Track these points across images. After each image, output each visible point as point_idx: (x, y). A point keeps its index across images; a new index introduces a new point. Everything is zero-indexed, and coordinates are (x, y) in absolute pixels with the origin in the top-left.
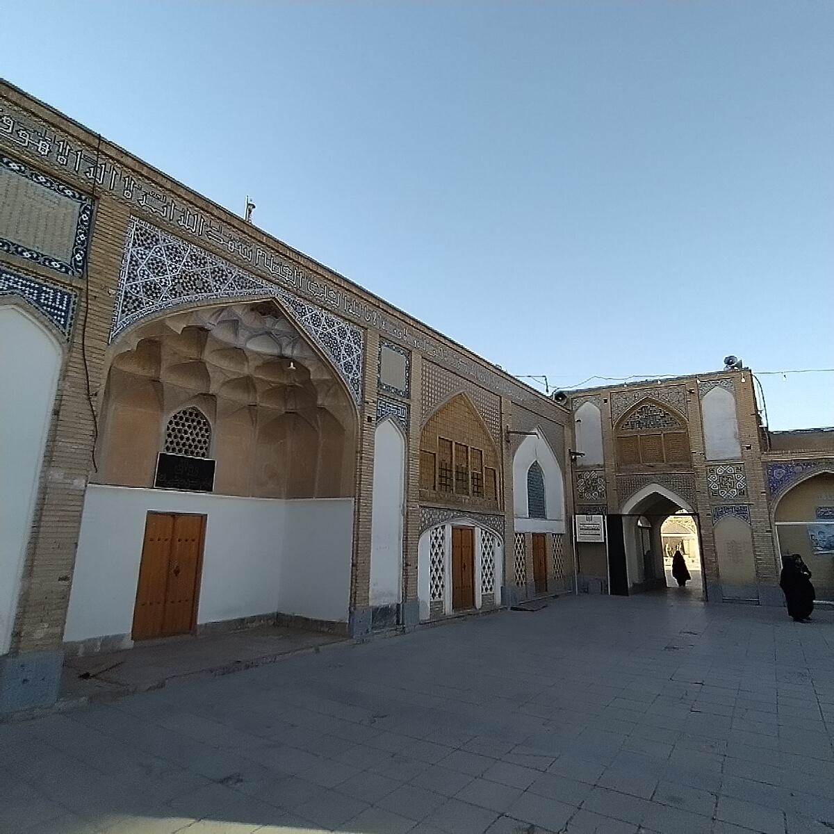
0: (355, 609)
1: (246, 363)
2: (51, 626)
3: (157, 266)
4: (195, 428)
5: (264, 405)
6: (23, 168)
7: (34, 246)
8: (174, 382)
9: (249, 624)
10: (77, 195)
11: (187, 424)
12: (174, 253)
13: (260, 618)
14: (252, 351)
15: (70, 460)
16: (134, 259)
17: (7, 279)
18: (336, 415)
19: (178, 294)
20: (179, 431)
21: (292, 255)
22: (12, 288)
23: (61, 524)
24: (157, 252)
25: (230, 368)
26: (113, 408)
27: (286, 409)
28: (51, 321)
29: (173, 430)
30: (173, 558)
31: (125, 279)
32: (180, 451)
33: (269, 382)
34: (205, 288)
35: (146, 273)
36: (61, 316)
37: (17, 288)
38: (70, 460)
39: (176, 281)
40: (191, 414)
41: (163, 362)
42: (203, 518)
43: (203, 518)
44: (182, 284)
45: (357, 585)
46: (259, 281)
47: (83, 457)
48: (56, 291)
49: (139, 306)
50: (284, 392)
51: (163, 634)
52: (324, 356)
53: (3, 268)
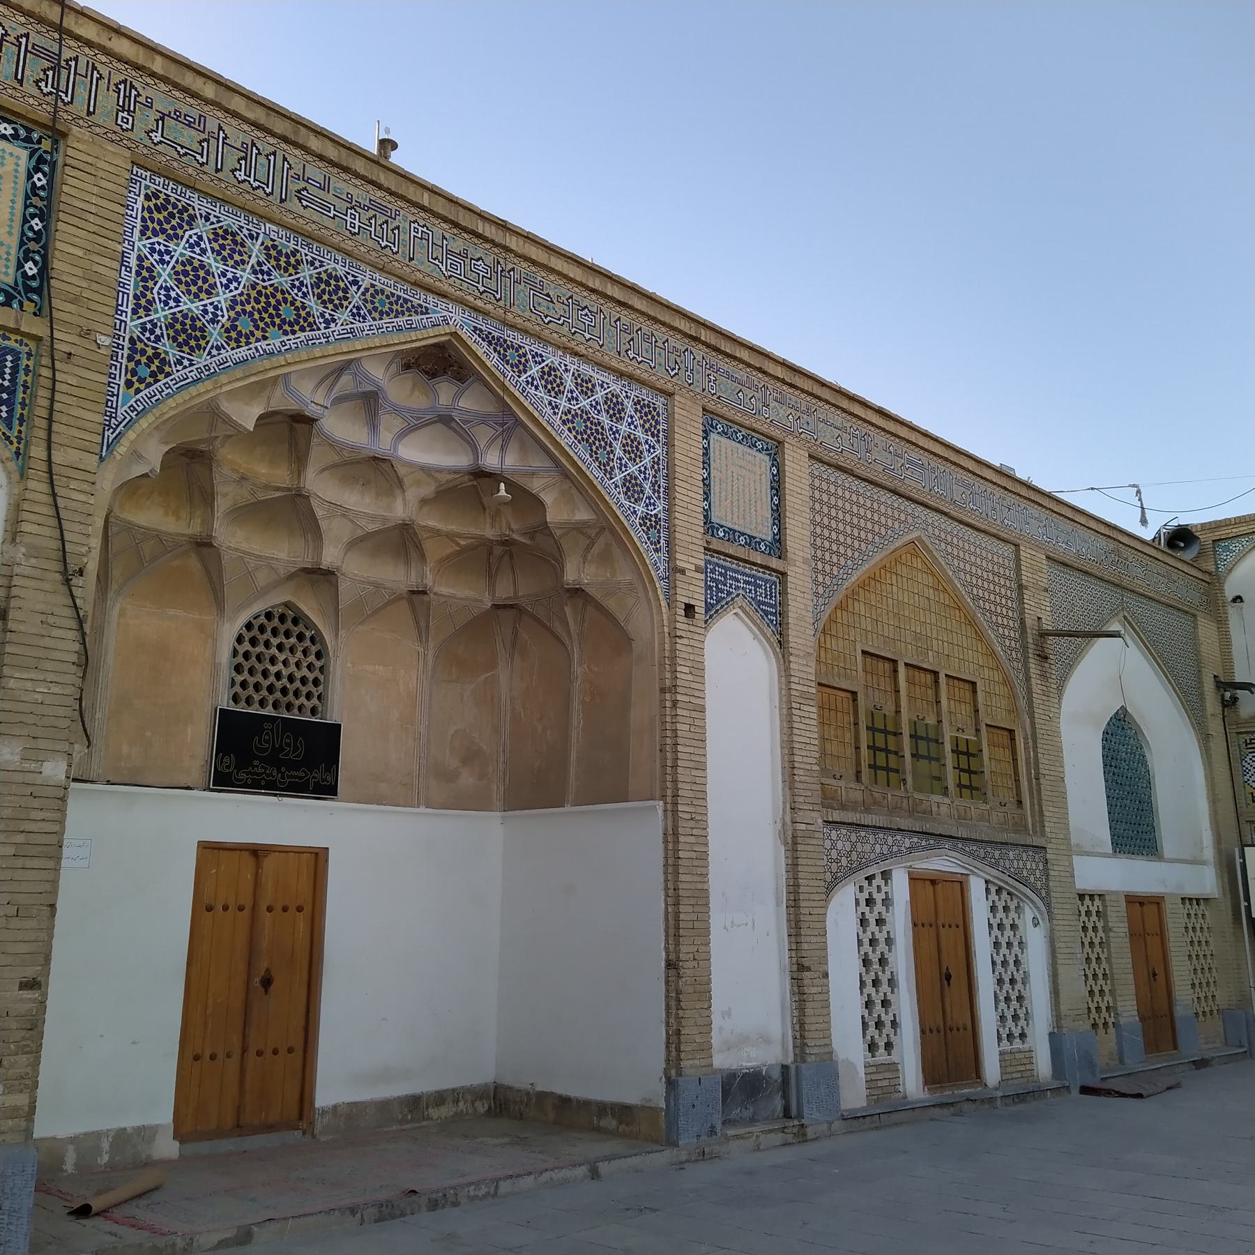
1: (398, 492)
5: (444, 590)
8: (244, 546)
10: (22, 132)
12: (229, 244)
14: (410, 464)
15: (30, 719)
18: (610, 604)
21: (490, 231)
23: (19, 862)
26: (116, 612)
29: (247, 655)
31: (129, 311)
32: (249, 701)
34: (303, 321)
40: (282, 618)
42: (318, 857)
43: (318, 857)
44: (251, 314)
46: (419, 298)
49: (161, 370)
50: (489, 558)
51: (240, 1129)
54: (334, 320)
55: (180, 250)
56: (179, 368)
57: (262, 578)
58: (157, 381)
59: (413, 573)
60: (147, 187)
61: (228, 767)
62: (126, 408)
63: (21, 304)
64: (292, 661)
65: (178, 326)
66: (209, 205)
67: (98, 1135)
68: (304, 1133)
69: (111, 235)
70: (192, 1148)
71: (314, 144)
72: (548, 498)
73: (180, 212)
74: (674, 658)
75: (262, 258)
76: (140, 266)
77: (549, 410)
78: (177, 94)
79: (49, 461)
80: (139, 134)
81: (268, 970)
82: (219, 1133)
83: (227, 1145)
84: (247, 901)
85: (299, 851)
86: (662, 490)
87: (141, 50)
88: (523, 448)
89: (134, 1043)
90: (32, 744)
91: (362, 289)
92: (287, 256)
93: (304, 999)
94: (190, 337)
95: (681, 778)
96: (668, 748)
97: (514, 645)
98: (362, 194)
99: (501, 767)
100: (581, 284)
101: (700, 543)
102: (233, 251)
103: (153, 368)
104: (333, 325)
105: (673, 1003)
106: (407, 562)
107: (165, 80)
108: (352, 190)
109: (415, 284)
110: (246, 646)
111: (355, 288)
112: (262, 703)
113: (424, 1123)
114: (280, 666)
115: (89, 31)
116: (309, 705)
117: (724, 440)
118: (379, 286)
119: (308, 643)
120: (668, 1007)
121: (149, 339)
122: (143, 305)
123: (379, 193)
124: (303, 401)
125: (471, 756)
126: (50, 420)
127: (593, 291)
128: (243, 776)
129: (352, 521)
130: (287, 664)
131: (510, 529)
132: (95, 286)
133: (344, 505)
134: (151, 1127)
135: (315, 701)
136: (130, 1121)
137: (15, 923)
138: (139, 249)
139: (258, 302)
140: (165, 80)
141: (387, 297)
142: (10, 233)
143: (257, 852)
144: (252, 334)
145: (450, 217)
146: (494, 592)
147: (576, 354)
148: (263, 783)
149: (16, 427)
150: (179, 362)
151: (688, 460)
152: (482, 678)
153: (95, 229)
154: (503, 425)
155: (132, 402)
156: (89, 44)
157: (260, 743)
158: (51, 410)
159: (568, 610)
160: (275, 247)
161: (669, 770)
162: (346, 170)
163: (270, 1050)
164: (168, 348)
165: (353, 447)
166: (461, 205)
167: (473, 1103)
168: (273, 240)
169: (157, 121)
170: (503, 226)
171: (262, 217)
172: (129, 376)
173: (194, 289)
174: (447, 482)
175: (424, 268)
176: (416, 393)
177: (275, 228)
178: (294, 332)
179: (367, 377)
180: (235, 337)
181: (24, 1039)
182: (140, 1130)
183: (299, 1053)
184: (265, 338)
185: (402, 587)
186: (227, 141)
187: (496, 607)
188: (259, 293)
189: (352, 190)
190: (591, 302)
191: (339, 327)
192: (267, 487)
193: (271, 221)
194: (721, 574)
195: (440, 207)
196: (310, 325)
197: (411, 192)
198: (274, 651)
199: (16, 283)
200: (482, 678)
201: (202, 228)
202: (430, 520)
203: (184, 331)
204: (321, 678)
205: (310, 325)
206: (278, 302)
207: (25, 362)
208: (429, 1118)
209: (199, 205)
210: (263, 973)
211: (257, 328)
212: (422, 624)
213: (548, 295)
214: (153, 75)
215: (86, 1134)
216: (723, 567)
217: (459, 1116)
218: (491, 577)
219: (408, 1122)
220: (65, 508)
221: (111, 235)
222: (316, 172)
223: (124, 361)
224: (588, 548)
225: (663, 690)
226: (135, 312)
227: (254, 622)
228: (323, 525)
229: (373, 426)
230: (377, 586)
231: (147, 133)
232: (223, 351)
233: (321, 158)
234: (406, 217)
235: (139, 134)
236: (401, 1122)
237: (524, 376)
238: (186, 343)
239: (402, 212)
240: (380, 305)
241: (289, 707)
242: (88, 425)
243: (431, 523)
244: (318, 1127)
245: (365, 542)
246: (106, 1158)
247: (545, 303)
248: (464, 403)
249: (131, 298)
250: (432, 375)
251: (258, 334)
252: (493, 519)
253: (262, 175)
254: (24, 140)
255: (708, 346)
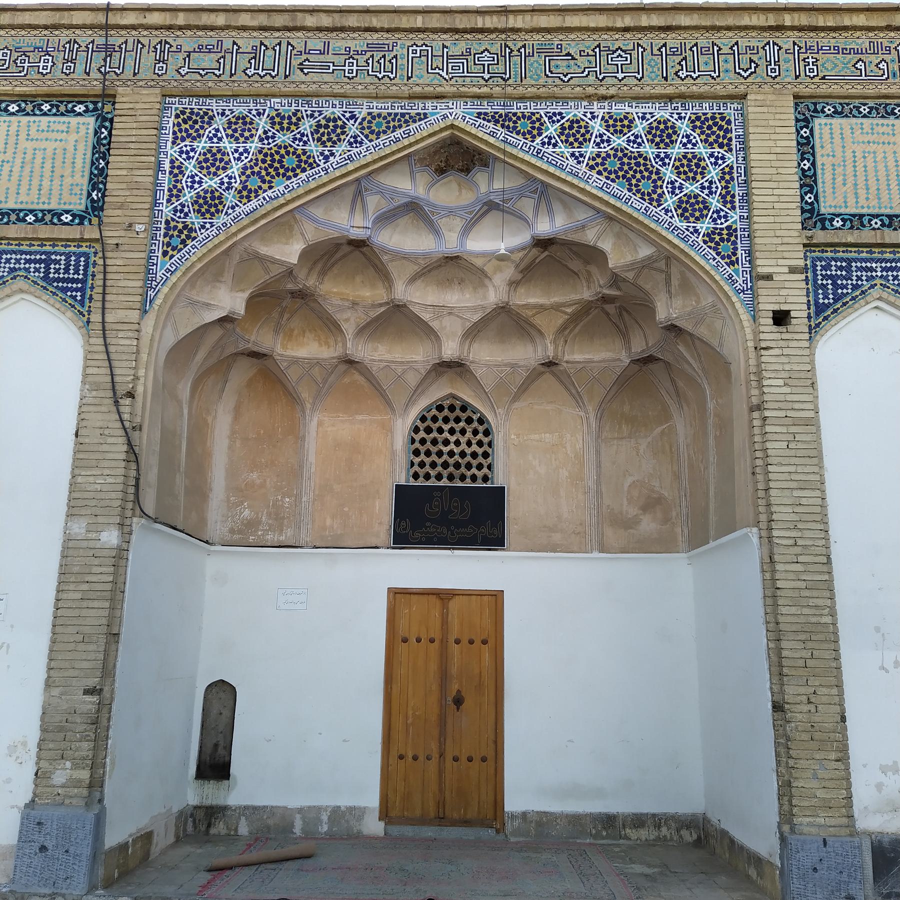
0: (792, 830)
1: (487, 281)
2: (75, 767)
3: (213, 161)
4: (463, 432)
5: (578, 357)
6: (23, 105)
7: (38, 203)
8: (387, 357)
9: (628, 831)
10: (91, 106)
11: (446, 427)
12: (240, 127)
13: (658, 821)
14: (483, 254)
15: (93, 503)
16: (176, 165)
17: (8, 261)
18: (702, 331)
19: (253, 195)
20: (434, 442)
21: (490, 22)
22: (15, 270)
23: (85, 604)
24: (216, 137)
25: (463, 302)
26: (314, 423)
27: (630, 356)
28: (64, 300)
29: (423, 441)
30: (445, 680)
31: (165, 202)
32: (427, 477)
33: (557, 307)
34: (306, 163)
35: (197, 179)
36: (77, 290)
37: (20, 269)
38: (93, 503)
39: (248, 172)
40: (452, 408)
41: (344, 326)
42: (496, 598)
43: (496, 598)
44: (259, 173)
45: (791, 762)
46: (418, 107)
47: (113, 495)
48: (68, 256)
49: (188, 237)
50: (586, 320)
51: (441, 820)
52: (607, 203)
53: (3, 247)
54: (332, 154)
55: (202, 145)
56: (203, 231)
57: (412, 379)
58: (185, 246)
59: (539, 349)
60: (176, 109)
61: (405, 529)
62: (163, 271)
63: (90, 221)
64: (463, 440)
65: (201, 201)
66: (225, 104)
67: (319, 809)
68: (498, 831)
69: (147, 152)
70: (395, 830)
71: (310, 21)
72: (606, 245)
73: (202, 117)
74: (759, 373)
75: (268, 127)
76: (173, 167)
77: (572, 162)
78: (200, 33)
79: (103, 322)
80: (172, 73)
81: (459, 691)
82: (422, 821)
83: (429, 832)
84: (436, 633)
85: (480, 594)
86: (737, 199)
87: (168, 14)
88: (565, 206)
89: (344, 741)
90: (94, 520)
91: (359, 120)
92: (289, 118)
93: (494, 714)
94: (210, 206)
95: (773, 500)
96: (758, 470)
97: (678, 395)
98: (357, 43)
99: (684, 510)
100: (608, 29)
101: (798, 240)
102: (244, 130)
103: (183, 237)
104: (331, 158)
105: (782, 750)
106: (532, 340)
107: (188, 27)
108: (350, 44)
109: (411, 97)
110: (422, 434)
111: (352, 122)
112: (439, 477)
113: (621, 841)
114: (452, 446)
115: (130, 19)
116: (480, 474)
117: (837, 121)
118: (375, 111)
119: (475, 424)
120: (777, 755)
121: (180, 217)
122: (175, 193)
123: (376, 36)
124: (344, 230)
125: (652, 503)
126: (104, 294)
127: (626, 29)
128: (417, 535)
129: (458, 316)
130: (460, 443)
131: (600, 286)
132: (135, 192)
133: (452, 307)
134: (360, 808)
135: (485, 470)
136: (344, 802)
137: (81, 647)
138: (171, 155)
139: (264, 161)
140: (188, 27)
141: (385, 118)
142: (83, 176)
143: (444, 596)
144: (260, 187)
145: (446, 26)
146: (630, 348)
147: (604, 98)
148: (435, 540)
149: (87, 303)
150: (203, 227)
151: (773, 157)
152: (659, 429)
153: (135, 152)
154: (535, 192)
155: (168, 266)
156: (134, 27)
157: (431, 508)
158: (104, 286)
159: (681, 348)
160: (278, 115)
161: (761, 494)
162: (342, 29)
163: (410, 755)
164: (194, 220)
165: (424, 255)
166: (456, 12)
167: (678, 830)
168: (277, 110)
169: (185, 59)
170: (504, 11)
171: (266, 96)
172: (165, 248)
173: (213, 170)
174: (522, 260)
175: (423, 80)
176: (464, 191)
177: (279, 100)
178: (296, 175)
179: (395, 191)
180: (245, 193)
181: (86, 730)
182: (351, 809)
183: (491, 762)
184: (270, 188)
185: (533, 362)
186: (241, 50)
187: (634, 362)
188: (266, 155)
189: (350, 44)
190: (626, 41)
191: (337, 158)
192: (374, 306)
193: (274, 96)
194: (841, 268)
195: (435, 22)
196: (310, 165)
197: (405, 22)
198: (446, 435)
199: (87, 208)
200: (659, 429)
201: (220, 123)
202: (529, 298)
203: (206, 203)
204: (490, 451)
205: (310, 165)
206: (282, 156)
207: (93, 259)
208: (627, 838)
209: (215, 106)
210: (454, 693)
211: (264, 182)
212: (574, 391)
213: (568, 54)
214: (180, 28)
215: (309, 807)
216: (842, 260)
217: (661, 841)
218: (624, 335)
219: (603, 838)
220: (116, 352)
221: (147, 152)
222: (315, 43)
223: (161, 239)
224: (668, 282)
225: (752, 410)
226: (168, 201)
227: (427, 415)
228: (435, 325)
229: (436, 231)
230: (513, 366)
231: (177, 71)
232: (237, 208)
233: (320, 29)
234: (402, 46)
235: (172, 73)
236: (595, 837)
237: (538, 140)
238: (208, 211)
239: (399, 42)
240: (373, 127)
241: (463, 478)
242: (130, 291)
243: (532, 300)
244: (509, 827)
245: (473, 333)
246: (325, 828)
247: (565, 63)
248: (497, 185)
249: (166, 191)
250: (467, 170)
251: (265, 186)
252: (588, 281)
253: (269, 65)
254: (93, 111)
255: (800, 29)
